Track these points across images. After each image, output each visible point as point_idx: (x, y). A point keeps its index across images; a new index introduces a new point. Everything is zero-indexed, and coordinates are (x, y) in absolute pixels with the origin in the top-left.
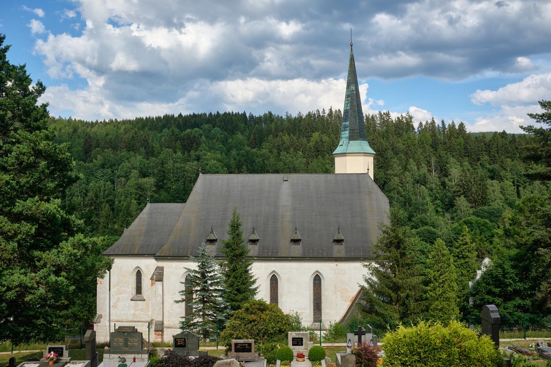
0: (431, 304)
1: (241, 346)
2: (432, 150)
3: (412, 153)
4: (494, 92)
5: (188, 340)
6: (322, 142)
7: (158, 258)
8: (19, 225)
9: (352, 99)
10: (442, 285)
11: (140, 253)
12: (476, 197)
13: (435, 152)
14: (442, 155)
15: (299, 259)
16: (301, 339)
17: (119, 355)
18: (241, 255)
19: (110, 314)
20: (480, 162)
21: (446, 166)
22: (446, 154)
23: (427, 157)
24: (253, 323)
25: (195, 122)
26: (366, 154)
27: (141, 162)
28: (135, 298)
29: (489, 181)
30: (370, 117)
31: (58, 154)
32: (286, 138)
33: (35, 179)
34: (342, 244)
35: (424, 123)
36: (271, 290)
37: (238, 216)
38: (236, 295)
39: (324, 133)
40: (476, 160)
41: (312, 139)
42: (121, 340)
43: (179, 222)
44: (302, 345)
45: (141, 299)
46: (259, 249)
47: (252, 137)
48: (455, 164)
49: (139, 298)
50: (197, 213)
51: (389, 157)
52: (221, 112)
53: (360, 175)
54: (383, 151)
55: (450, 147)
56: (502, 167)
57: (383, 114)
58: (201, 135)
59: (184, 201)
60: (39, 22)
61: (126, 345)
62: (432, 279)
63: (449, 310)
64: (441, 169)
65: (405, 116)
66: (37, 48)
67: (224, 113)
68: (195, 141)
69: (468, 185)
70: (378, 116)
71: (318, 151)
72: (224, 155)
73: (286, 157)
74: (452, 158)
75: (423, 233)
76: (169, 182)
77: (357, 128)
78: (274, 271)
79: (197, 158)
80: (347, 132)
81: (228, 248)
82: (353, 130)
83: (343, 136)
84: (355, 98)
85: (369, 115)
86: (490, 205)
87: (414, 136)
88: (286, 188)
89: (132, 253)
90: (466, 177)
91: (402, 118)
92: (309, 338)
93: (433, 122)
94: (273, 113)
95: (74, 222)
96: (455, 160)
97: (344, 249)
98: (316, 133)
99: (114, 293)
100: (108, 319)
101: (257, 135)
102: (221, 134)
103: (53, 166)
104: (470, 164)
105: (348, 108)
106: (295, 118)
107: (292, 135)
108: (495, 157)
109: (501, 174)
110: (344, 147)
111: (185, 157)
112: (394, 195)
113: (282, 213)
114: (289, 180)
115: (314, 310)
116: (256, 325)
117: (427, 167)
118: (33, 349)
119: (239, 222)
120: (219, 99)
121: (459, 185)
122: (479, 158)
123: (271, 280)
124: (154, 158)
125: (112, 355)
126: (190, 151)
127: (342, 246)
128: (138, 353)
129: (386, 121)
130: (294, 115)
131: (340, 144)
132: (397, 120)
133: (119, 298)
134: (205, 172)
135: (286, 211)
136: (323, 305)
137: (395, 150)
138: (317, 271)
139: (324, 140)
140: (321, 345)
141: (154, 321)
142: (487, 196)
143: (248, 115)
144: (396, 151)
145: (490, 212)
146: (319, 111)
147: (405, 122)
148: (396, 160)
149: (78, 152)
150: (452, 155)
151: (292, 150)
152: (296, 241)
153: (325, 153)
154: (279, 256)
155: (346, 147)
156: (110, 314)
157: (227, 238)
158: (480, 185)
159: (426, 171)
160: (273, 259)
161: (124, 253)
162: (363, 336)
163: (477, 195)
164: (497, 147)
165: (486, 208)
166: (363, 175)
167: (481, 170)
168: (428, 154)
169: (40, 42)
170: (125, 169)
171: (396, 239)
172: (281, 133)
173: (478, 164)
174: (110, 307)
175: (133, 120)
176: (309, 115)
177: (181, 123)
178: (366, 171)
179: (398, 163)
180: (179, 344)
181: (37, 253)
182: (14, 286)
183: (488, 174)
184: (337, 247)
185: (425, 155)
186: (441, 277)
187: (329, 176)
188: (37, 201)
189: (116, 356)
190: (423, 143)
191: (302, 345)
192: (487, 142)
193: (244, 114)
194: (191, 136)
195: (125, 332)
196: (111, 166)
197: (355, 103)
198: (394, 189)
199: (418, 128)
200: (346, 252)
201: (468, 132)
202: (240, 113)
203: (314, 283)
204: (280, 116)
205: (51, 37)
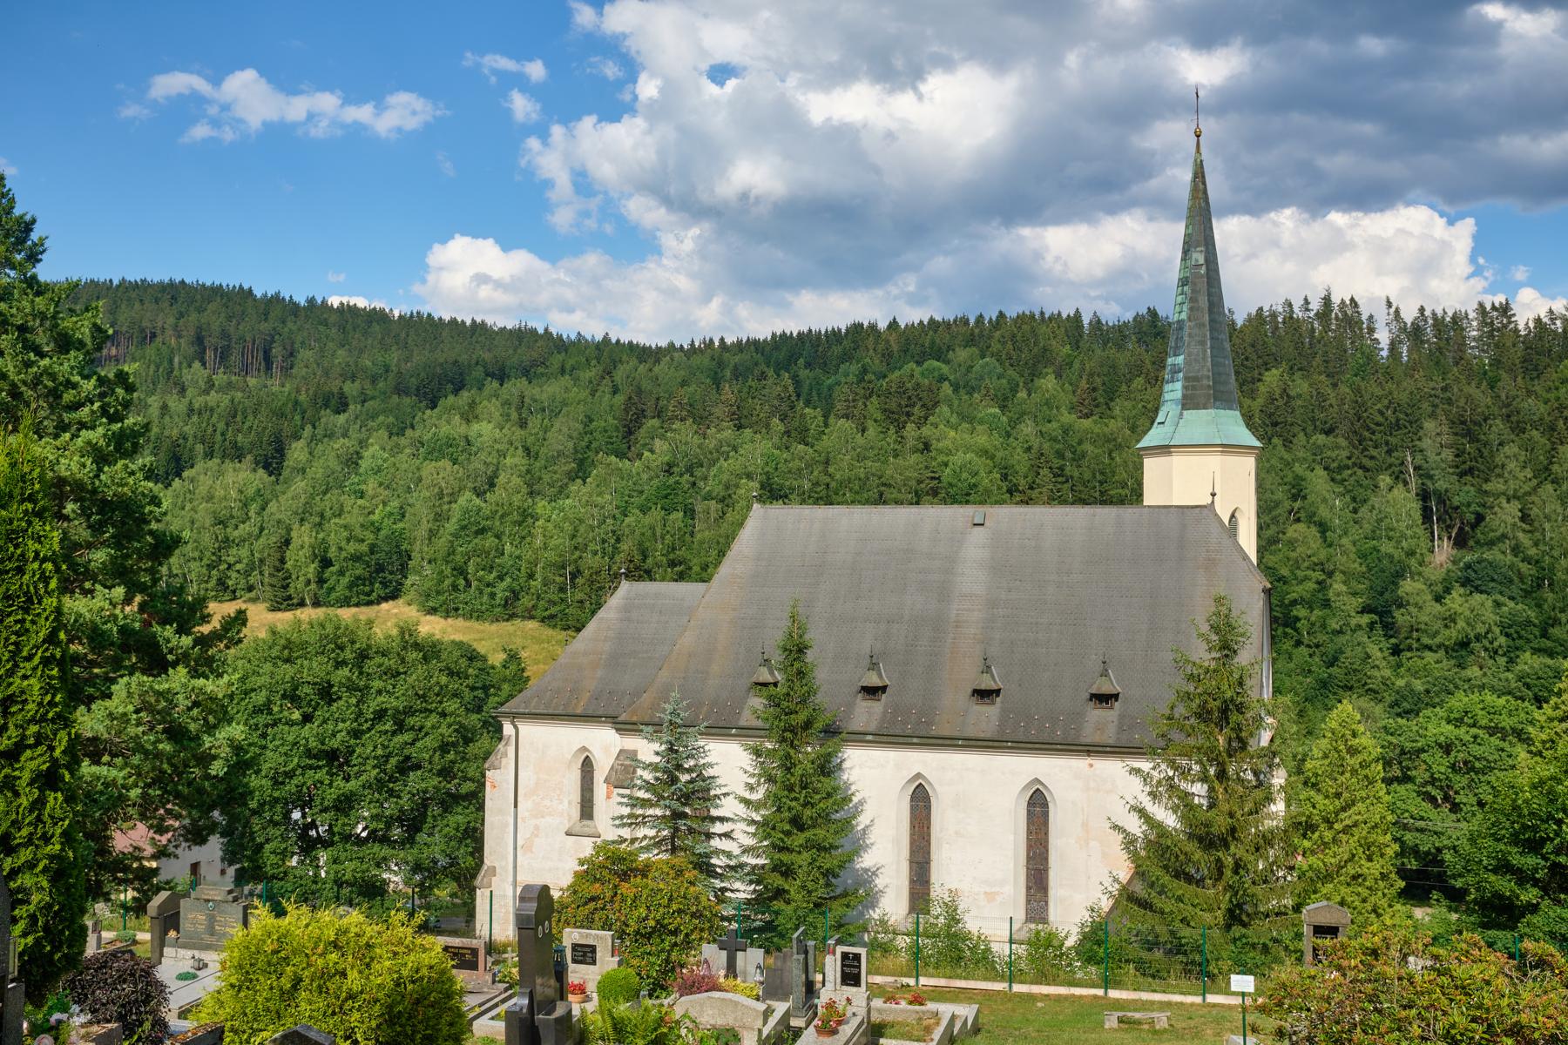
6: (1288, 396)
9: (1193, 291)
11: (590, 712)
16: (593, 949)
19: (515, 867)
25: (933, 342)
26: (1228, 448)
27: (769, 458)
28: (577, 829)
30: (1448, 319)
36: (913, 827)
38: (788, 833)
41: (1262, 388)
44: (594, 962)
45: (591, 831)
46: (885, 713)
49: (587, 830)
51: (1493, 437)
52: (1012, 312)
54: (1475, 423)
57: (1488, 307)
61: (211, 931)
68: (920, 399)
70: (1472, 315)
71: (1275, 424)
72: (997, 440)
75: (1539, 678)
78: (918, 775)
80: (1178, 385)
82: (1196, 379)
84: (1202, 285)
85: (1445, 313)
88: (976, 546)
89: (570, 711)
91: (1553, 320)
97: (1116, 723)
98: (1274, 371)
99: (527, 814)
100: (511, 879)
101: (1098, 380)
110: (1168, 428)
112: (1502, 557)
113: (958, 615)
115: (1028, 888)
120: (1017, 273)
123: (914, 797)
124: (801, 447)
125: (182, 952)
127: (1112, 712)
129: (1498, 330)
131: (1159, 419)
132: (1531, 325)
133: (537, 828)
135: (969, 610)
136: (1052, 874)
137: (1514, 419)
138: (1037, 781)
140: (1010, 987)
143: (1086, 321)
144: (1518, 422)
146: (1290, 305)
148: (1516, 450)
149: (606, 431)
152: (984, 695)
153: (1296, 429)
154: (933, 733)
155: (1172, 429)
156: (515, 867)
160: (915, 740)
161: (551, 711)
162: (740, 954)
166: (1197, 510)
169: (534, 143)
170: (725, 477)
174: (515, 848)
175: (765, 341)
177: (895, 348)
178: (1207, 500)
179: (1522, 459)
184: (1096, 714)
186: (1343, 815)
187: (1128, 512)
189: (189, 953)
191: (594, 962)
193: (1078, 315)
195: (209, 901)
196: (690, 470)
197: (1203, 302)
198: (1504, 536)
200: (1121, 729)
202: (1064, 316)
205: (557, 131)
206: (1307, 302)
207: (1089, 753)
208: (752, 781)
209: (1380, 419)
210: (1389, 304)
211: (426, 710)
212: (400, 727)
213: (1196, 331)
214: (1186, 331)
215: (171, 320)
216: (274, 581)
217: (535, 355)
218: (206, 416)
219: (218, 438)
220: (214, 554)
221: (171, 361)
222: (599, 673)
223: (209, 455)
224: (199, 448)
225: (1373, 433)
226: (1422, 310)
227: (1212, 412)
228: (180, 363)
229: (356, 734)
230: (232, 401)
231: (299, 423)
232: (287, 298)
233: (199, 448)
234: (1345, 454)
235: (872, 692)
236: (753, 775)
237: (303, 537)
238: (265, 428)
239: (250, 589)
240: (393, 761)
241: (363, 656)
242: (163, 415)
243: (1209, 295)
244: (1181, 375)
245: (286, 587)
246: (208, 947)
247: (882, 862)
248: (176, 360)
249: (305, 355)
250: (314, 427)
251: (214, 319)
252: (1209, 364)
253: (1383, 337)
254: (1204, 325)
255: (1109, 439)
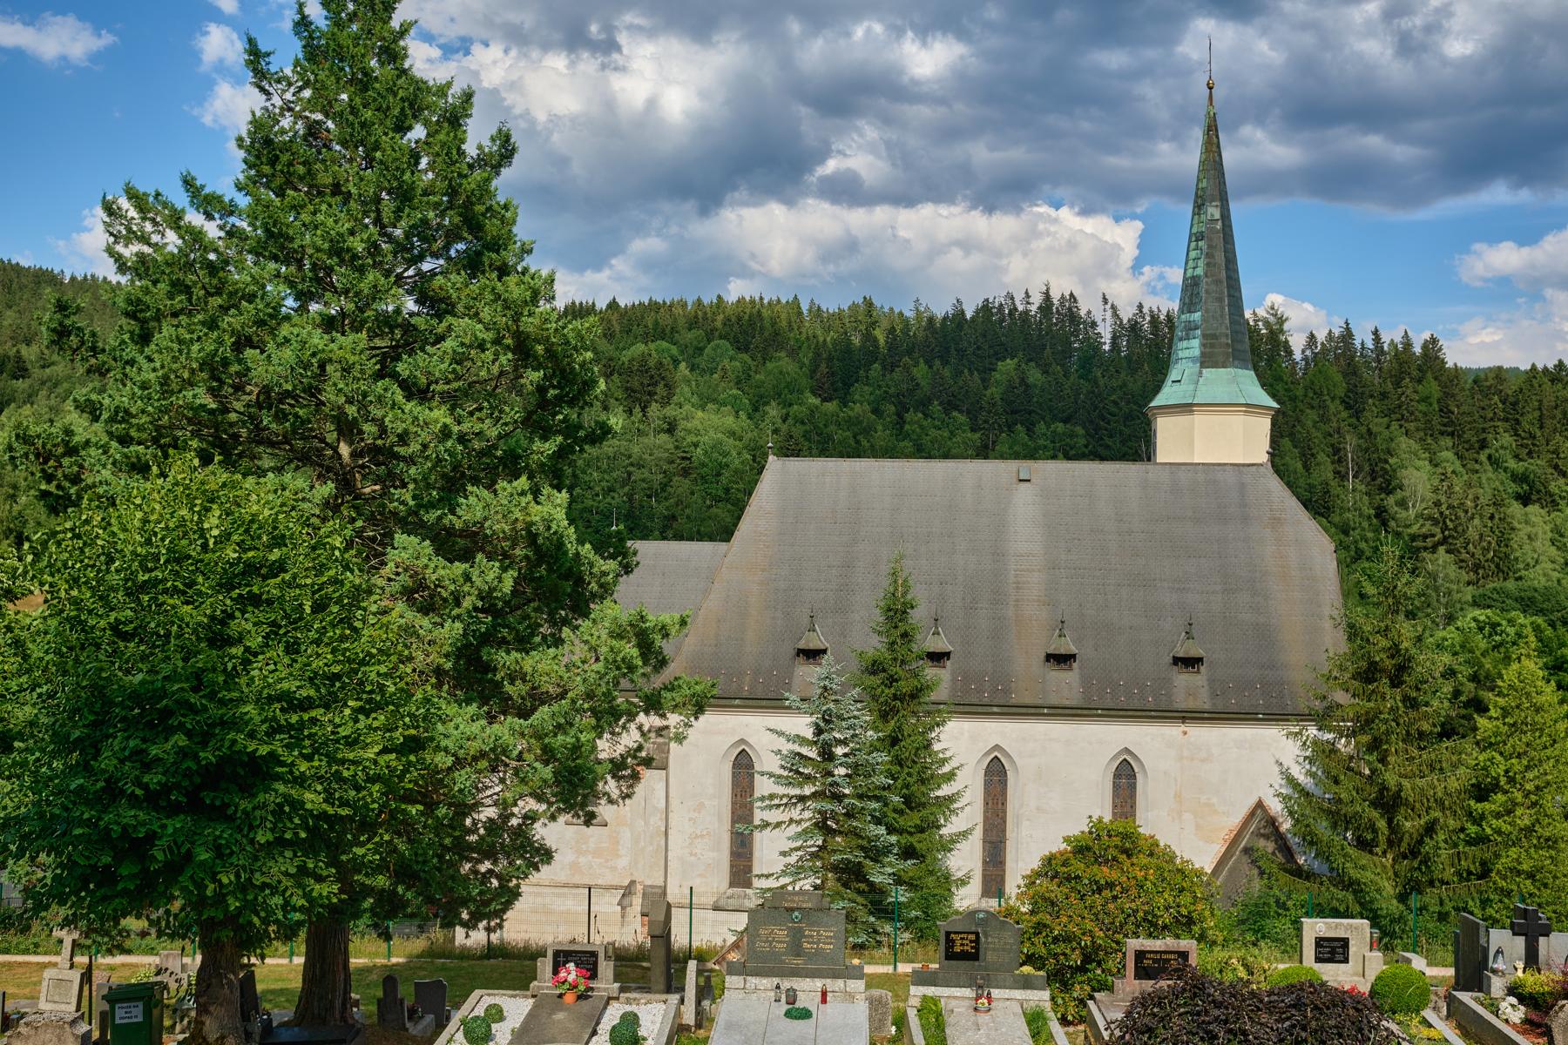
0: (1497, 856)
1: (1155, 961)
2: (1344, 414)
3: (1287, 423)
4: (1525, 251)
5: (986, 937)
8: (467, 565)
9: (1210, 247)
10: (1533, 798)
12: (1478, 552)
13: (1354, 420)
14: (1375, 429)
15: (1074, 712)
17: (776, 980)
18: (915, 695)
20: (1487, 451)
21: (1386, 462)
22: (1388, 427)
23: (1331, 435)
24: (1107, 893)
25: (656, 323)
26: (1252, 408)
29: (1515, 508)
31: (575, 348)
32: (920, 371)
33: (506, 424)
34: (1198, 672)
35: (1321, 336)
37: (905, 581)
39: (1030, 360)
40: (1476, 445)
42: (782, 933)
43: (712, 596)
44: (1346, 961)
46: (954, 680)
47: (823, 368)
48: (1416, 455)
50: (763, 570)
53: (1245, 470)
55: (1400, 407)
56: (1556, 467)
58: (676, 362)
59: (725, 533)
60: (227, 30)
61: (796, 950)
62: (1503, 781)
63: (1555, 877)
64: (1373, 471)
65: (1265, 315)
66: (218, 105)
67: (739, 301)
68: (663, 379)
69: (1457, 518)
73: (921, 427)
74: (1403, 439)
76: (588, 494)
77: (1224, 331)
78: (997, 747)
79: (666, 426)
80: (1196, 343)
81: (874, 673)
82: (1214, 336)
83: (1181, 354)
84: (1218, 241)
86: (1520, 578)
87: (1294, 373)
90: (1450, 492)
92: (1368, 939)
93: (1348, 335)
94: (877, 303)
95: (591, 565)
96: (1415, 446)
97: (1207, 688)
102: (732, 359)
103: (554, 387)
104: (1460, 457)
105: (1199, 271)
106: (945, 318)
107: (937, 362)
108: (1534, 438)
109: (1553, 487)
111: (633, 423)
113: (1016, 576)
114: (1033, 480)
116: (1115, 898)
117: (1333, 463)
119: (909, 597)
121: (1430, 518)
122: (1485, 439)
125: (753, 981)
126: (646, 407)
128: (835, 975)
130: (941, 308)
134: (789, 450)
138: (1127, 750)
139: (1031, 380)
141: (639, 887)
142: (1513, 550)
143: (805, 308)
145: (1522, 599)
147: (1264, 331)
150: (1403, 430)
151: (936, 407)
152: (1061, 660)
154: (1013, 702)
155: (1192, 387)
157: (874, 645)
158: (1492, 517)
159: (1330, 475)
160: (995, 709)
162: (1542, 939)
163: (1484, 549)
164: (1540, 409)
165: (1510, 585)
167: (1490, 475)
168: (1335, 424)
171: (1392, 657)
172: (906, 359)
173: (1483, 457)
176: (986, 308)
177: (617, 328)
180: (958, 949)
181: (505, 659)
182: (472, 753)
183: (1513, 487)
184: (1183, 680)
185: (1327, 428)
186: (1530, 775)
188: (523, 493)
189: (766, 983)
190: (1319, 394)
191: (1346, 961)
192: (1510, 392)
194: (652, 363)
195: (792, 910)
197: (1220, 258)
199: (1303, 352)
200: (1214, 695)
201: (1450, 364)
202: (784, 301)
203: (1116, 786)
204: (897, 311)
206: (1027, 295)
207: (1184, 720)
209: (1115, 410)
210: (1105, 301)
213: (1213, 287)
214: (1203, 287)
225: (1108, 423)
226: (1140, 307)
234: (1083, 441)
244: (1198, 332)
246: (795, 973)
252: (1227, 322)
253: (1105, 332)
254: (1221, 282)
255: (851, 422)
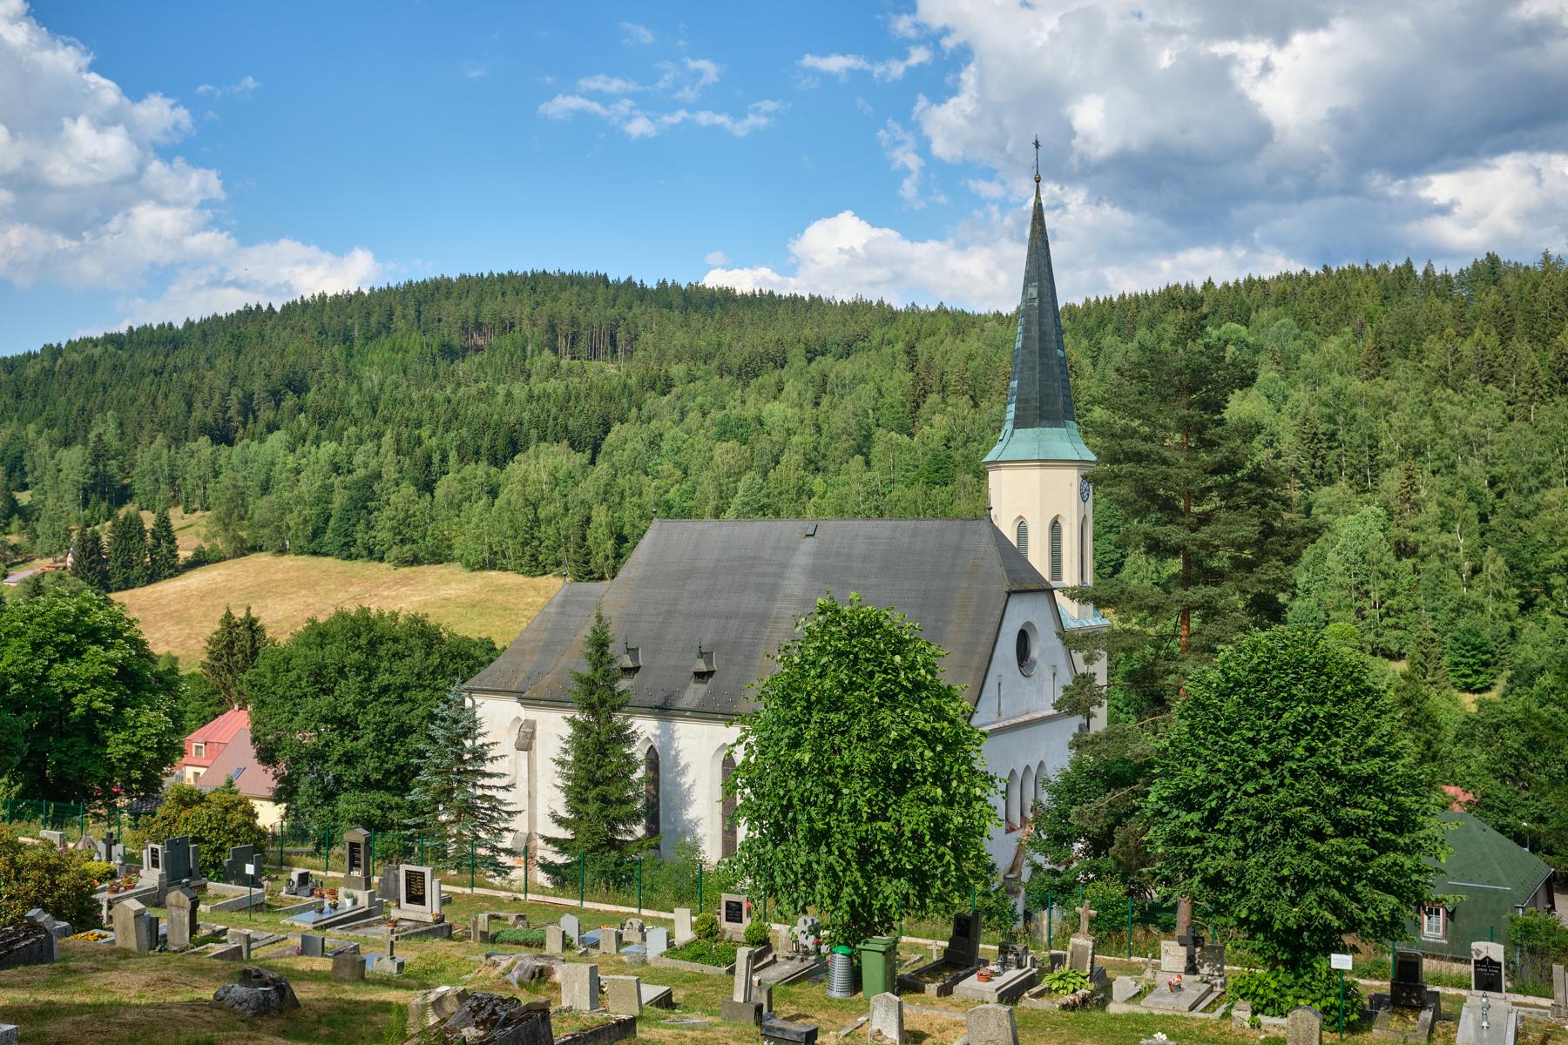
7: (527, 701)
82: (1027, 401)
118: (1489, 883)
123: (724, 763)
208: (567, 746)
211: (421, 686)
212: (401, 701)
215: (527, 310)
216: (577, 557)
217: (859, 330)
218: (543, 400)
219: (551, 422)
220: (526, 532)
221: (524, 350)
222: (536, 657)
223: (542, 438)
224: (534, 432)
227: (1037, 430)
228: (533, 351)
229: (361, 704)
230: (567, 387)
231: (626, 406)
232: (638, 283)
233: (534, 432)
235: (701, 676)
236: (567, 742)
237: (600, 515)
238: (594, 412)
239: (558, 564)
240: (392, 726)
241: (373, 644)
242: (506, 402)
243: (1040, 325)
245: (587, 563)
247: (701, 815)
248: (529, 348)
249: (646, 337)
250: (640, 409)
251: (564, 307)
